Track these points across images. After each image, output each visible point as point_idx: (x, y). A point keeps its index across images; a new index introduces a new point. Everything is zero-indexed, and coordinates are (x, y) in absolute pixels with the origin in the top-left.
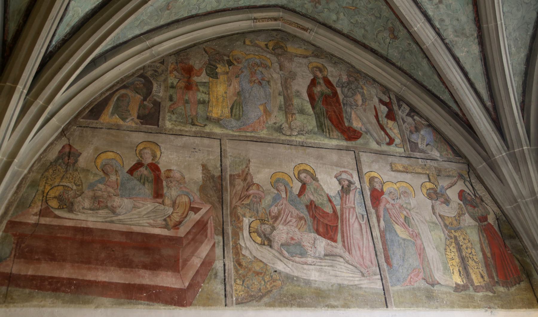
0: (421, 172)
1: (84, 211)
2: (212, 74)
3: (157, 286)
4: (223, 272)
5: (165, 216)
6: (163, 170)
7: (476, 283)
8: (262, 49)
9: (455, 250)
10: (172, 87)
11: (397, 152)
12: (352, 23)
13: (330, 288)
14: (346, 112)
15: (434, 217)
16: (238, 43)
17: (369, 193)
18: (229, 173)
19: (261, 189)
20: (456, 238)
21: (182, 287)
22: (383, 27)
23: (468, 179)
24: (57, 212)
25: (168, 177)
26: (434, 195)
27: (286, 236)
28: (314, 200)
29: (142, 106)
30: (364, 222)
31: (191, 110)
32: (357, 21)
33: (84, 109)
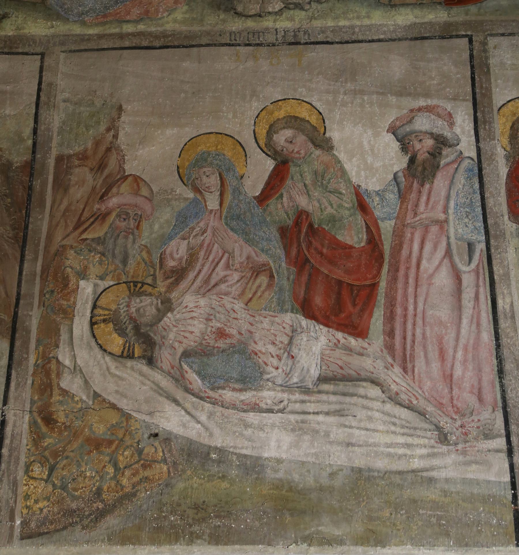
13: (325, 481)
17: (503, 170)
18: (54, 153)
19: (144, 192)
27: (202, 326)
28: (310, 209)
30: (473, 266)
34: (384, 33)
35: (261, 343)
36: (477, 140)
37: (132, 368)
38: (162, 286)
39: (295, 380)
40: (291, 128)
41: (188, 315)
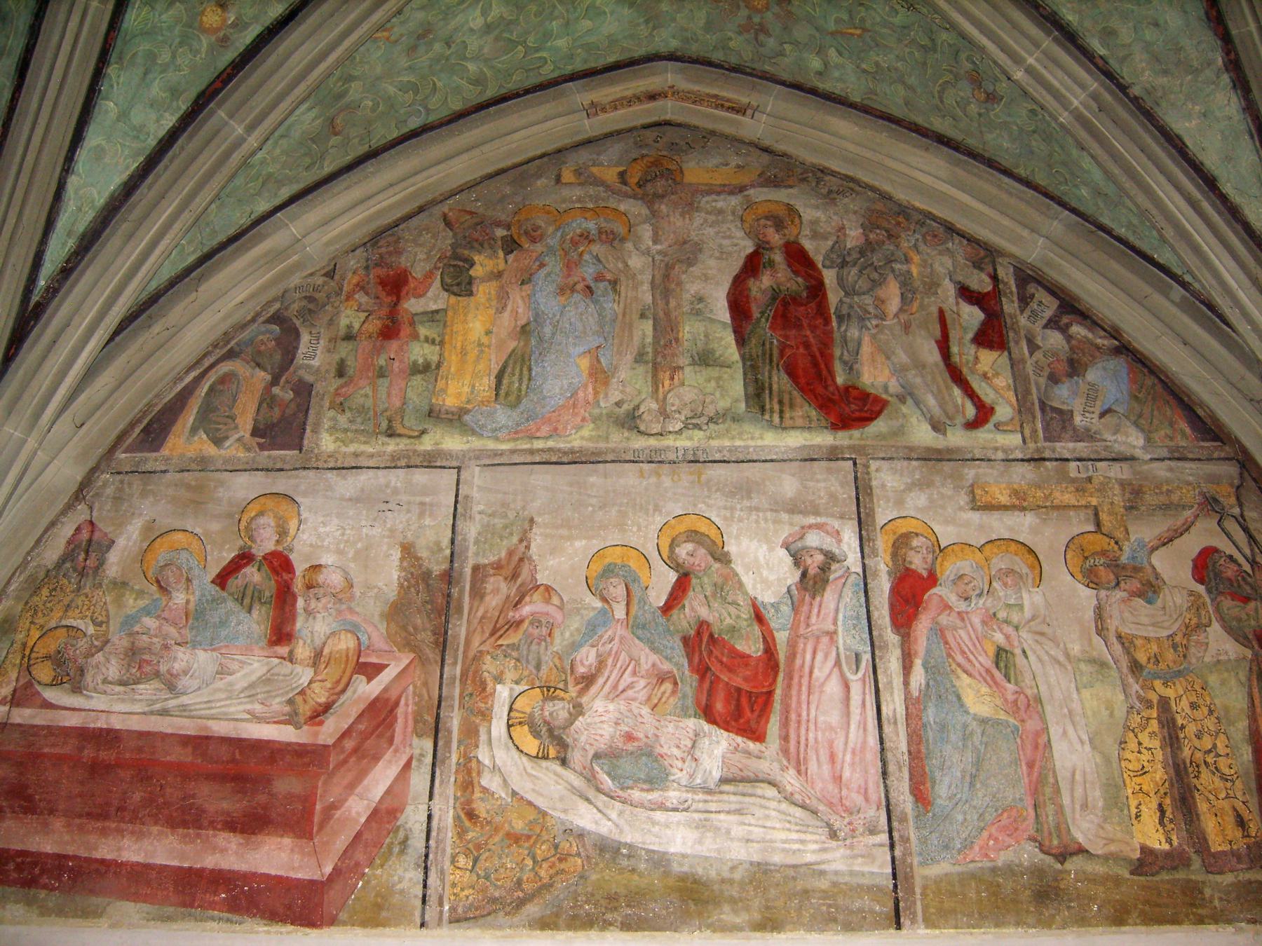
0: (1073, 502)
1: (109, 688)
2: (458, 284)
3: (254, 874)
4: (424, 835)
5: (293, 689)
6: (300, 567)
7: (1217, 844)
8: (608, 188)
9: (1156, 743)
10: (349, 337)
11: (996, 449)
12: (864, 71)
13: (726, 874)
14: (845, 340)
15: (1097, 640)
16: (541, 183)
19: (555, 600)
20: (1164, 703)
21: (315, 878)
22: (951, 72)
23: (1236, 511)
24: (50, 695)
25: (309, 587)
26: (1106, 568)
28: (711, 619)
29: (267, 400)
30: (860, 674)
31: (389, 395)
32: (877, 64)
33: (132, 425)
34: (777, 453)
35: (666, 747)
36: (863, 557)
37: (547, 769)
38: (573, 691)
39: (698, 781)
40: (693, 541)
41: (597, 719)
